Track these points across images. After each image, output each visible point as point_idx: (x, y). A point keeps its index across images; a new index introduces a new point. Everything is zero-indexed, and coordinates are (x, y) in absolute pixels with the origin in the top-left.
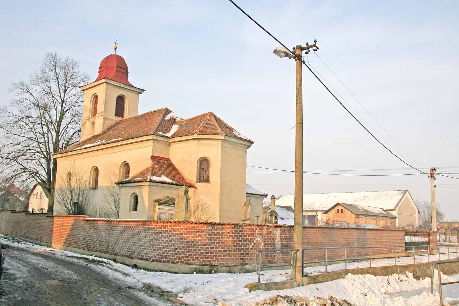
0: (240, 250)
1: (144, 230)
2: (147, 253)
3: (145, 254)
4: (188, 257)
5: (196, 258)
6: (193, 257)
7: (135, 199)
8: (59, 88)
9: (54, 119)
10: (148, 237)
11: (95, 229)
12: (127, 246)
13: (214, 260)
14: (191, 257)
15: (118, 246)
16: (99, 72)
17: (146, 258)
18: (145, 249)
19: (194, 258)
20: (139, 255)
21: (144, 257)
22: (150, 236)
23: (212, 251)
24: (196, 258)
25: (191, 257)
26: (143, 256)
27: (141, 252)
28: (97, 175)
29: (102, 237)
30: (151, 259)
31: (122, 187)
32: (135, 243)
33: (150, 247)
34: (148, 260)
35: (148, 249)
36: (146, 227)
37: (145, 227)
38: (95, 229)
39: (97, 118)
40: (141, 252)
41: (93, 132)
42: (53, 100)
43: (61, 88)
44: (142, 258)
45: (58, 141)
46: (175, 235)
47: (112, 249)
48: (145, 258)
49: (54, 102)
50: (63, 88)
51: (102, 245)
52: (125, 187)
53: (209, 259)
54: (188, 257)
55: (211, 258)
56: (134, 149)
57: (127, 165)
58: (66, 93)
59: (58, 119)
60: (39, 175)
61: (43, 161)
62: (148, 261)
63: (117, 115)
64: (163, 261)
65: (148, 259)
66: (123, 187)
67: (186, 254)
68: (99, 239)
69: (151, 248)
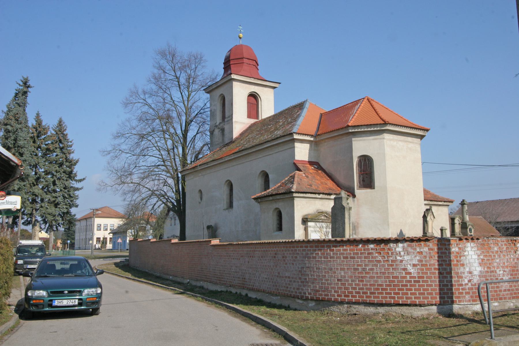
0: (413, 283)
1: (290, 254)
2: (298, 287)
3: (294, 288)
4: (359, 293)
5: (371, 293)
6: (366, 293)
7: (278, 216)
8: (181, 94)
9: (179, 132)
10: (296, 264)
11: (227, 256)
12: (269, 278)
13: (401, 295)
14: (364, 293)
15: (256, 278)
16: (224, 68)
17: (296, 294)
18: (295, 281)
19: (369, 294)
20: (286, 291)
21: (294, 294)
22: (300, 263)
23: (429, 273)
24: (371, 293)
25: (364, 293)
26: (292, 292)
27: (289, 286)
28: (231, 190)
29: (237, 267)
30: (303, 296)
31: (261, 202)
32: (279, 273)
33: (300, 278)
34: (300, 297)
35: (298, 282)
36: (293, 250)
37: (292, 250)
38: (227, 256)
39: (226, 123)
40: (289, 286)
41: (223, 140)
42: (175, 108)
43: (183, 94)
44: (291, 295)
45: (184, 155)
46: (335, 259)
47: (250, 282)
48: (294, 295)
49: (176, 111)
50: (187, 93)
51: (237, 278)
52: (265, 201)
53: (413, 290)
54: (359, 293)
55: (395, 294)
56: (273, 154)
57: (265, 176)
58: (191, 98)
59: (184, 129)
60: (168, 197)
61: (171, 181)
62: (27, 290)
63: (249, 116)
64: (292, 296)
65: (299, 296)
66: (262, 201)
67: (355, 288)
68: (233, 269)
69: (303, 280)
